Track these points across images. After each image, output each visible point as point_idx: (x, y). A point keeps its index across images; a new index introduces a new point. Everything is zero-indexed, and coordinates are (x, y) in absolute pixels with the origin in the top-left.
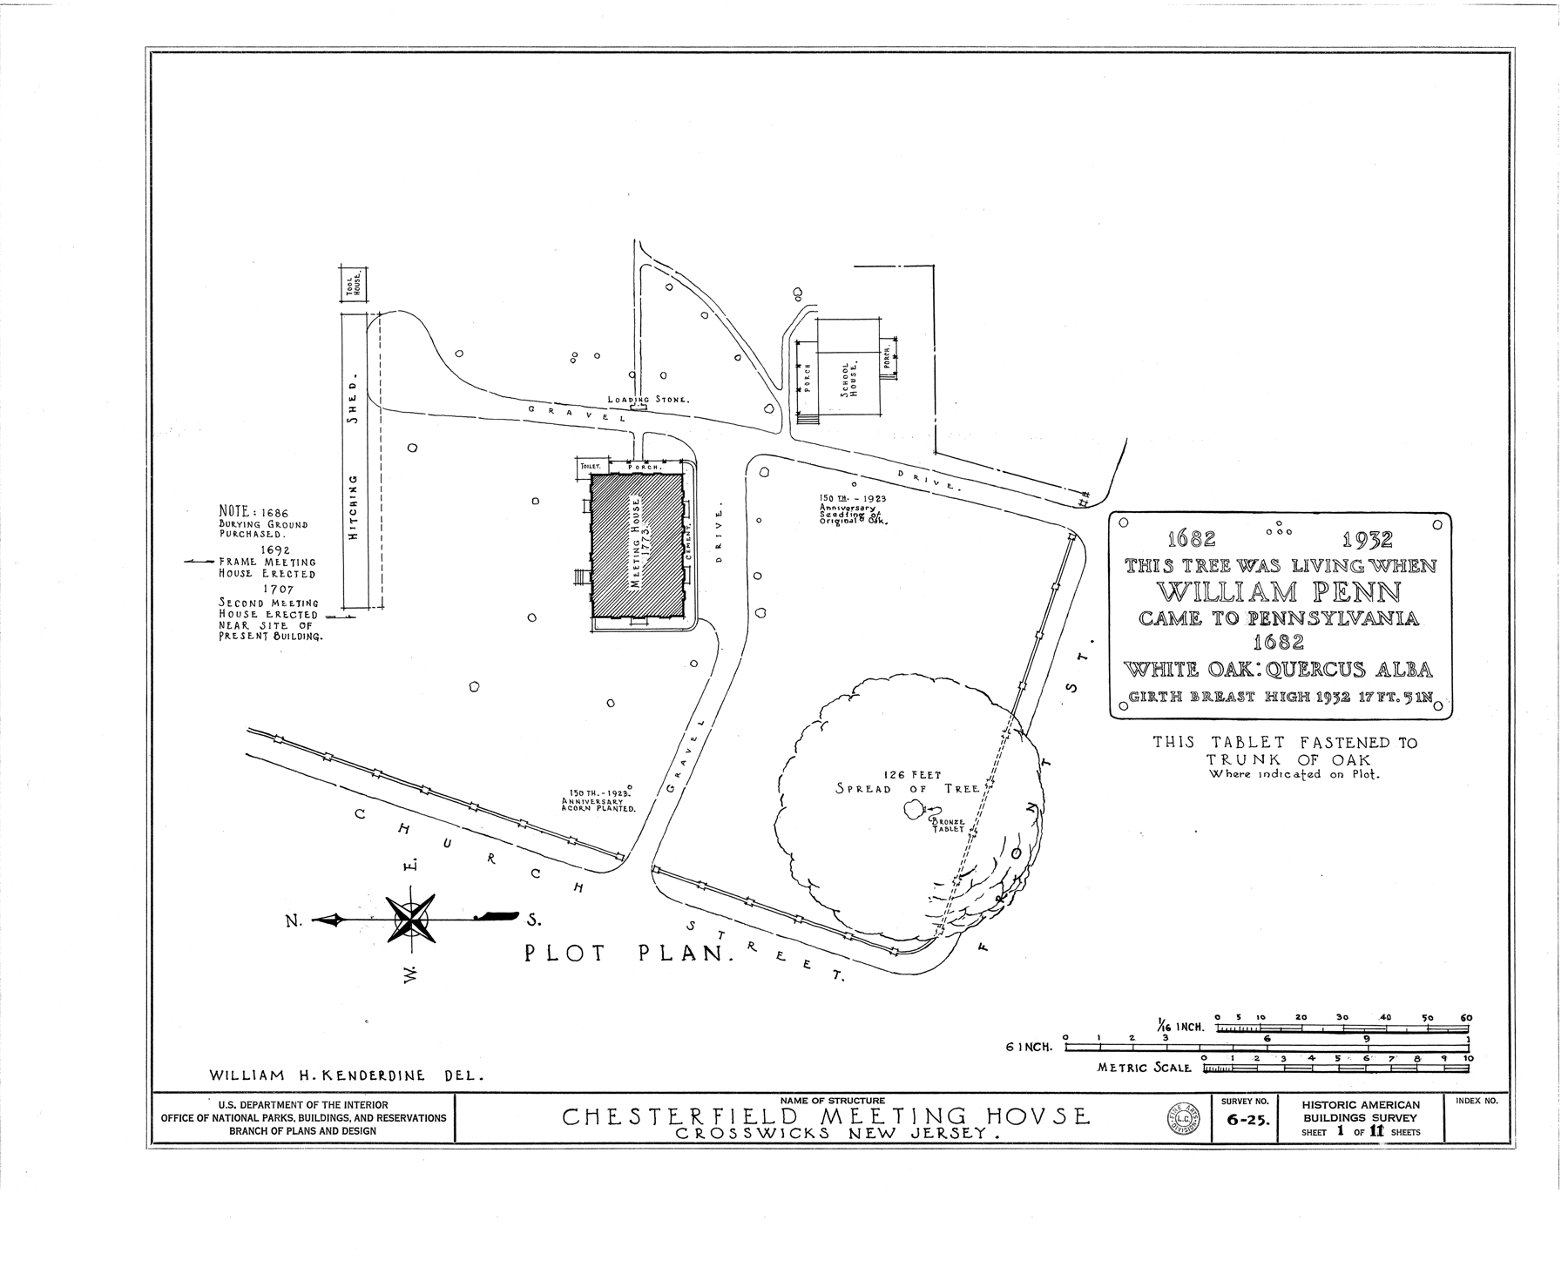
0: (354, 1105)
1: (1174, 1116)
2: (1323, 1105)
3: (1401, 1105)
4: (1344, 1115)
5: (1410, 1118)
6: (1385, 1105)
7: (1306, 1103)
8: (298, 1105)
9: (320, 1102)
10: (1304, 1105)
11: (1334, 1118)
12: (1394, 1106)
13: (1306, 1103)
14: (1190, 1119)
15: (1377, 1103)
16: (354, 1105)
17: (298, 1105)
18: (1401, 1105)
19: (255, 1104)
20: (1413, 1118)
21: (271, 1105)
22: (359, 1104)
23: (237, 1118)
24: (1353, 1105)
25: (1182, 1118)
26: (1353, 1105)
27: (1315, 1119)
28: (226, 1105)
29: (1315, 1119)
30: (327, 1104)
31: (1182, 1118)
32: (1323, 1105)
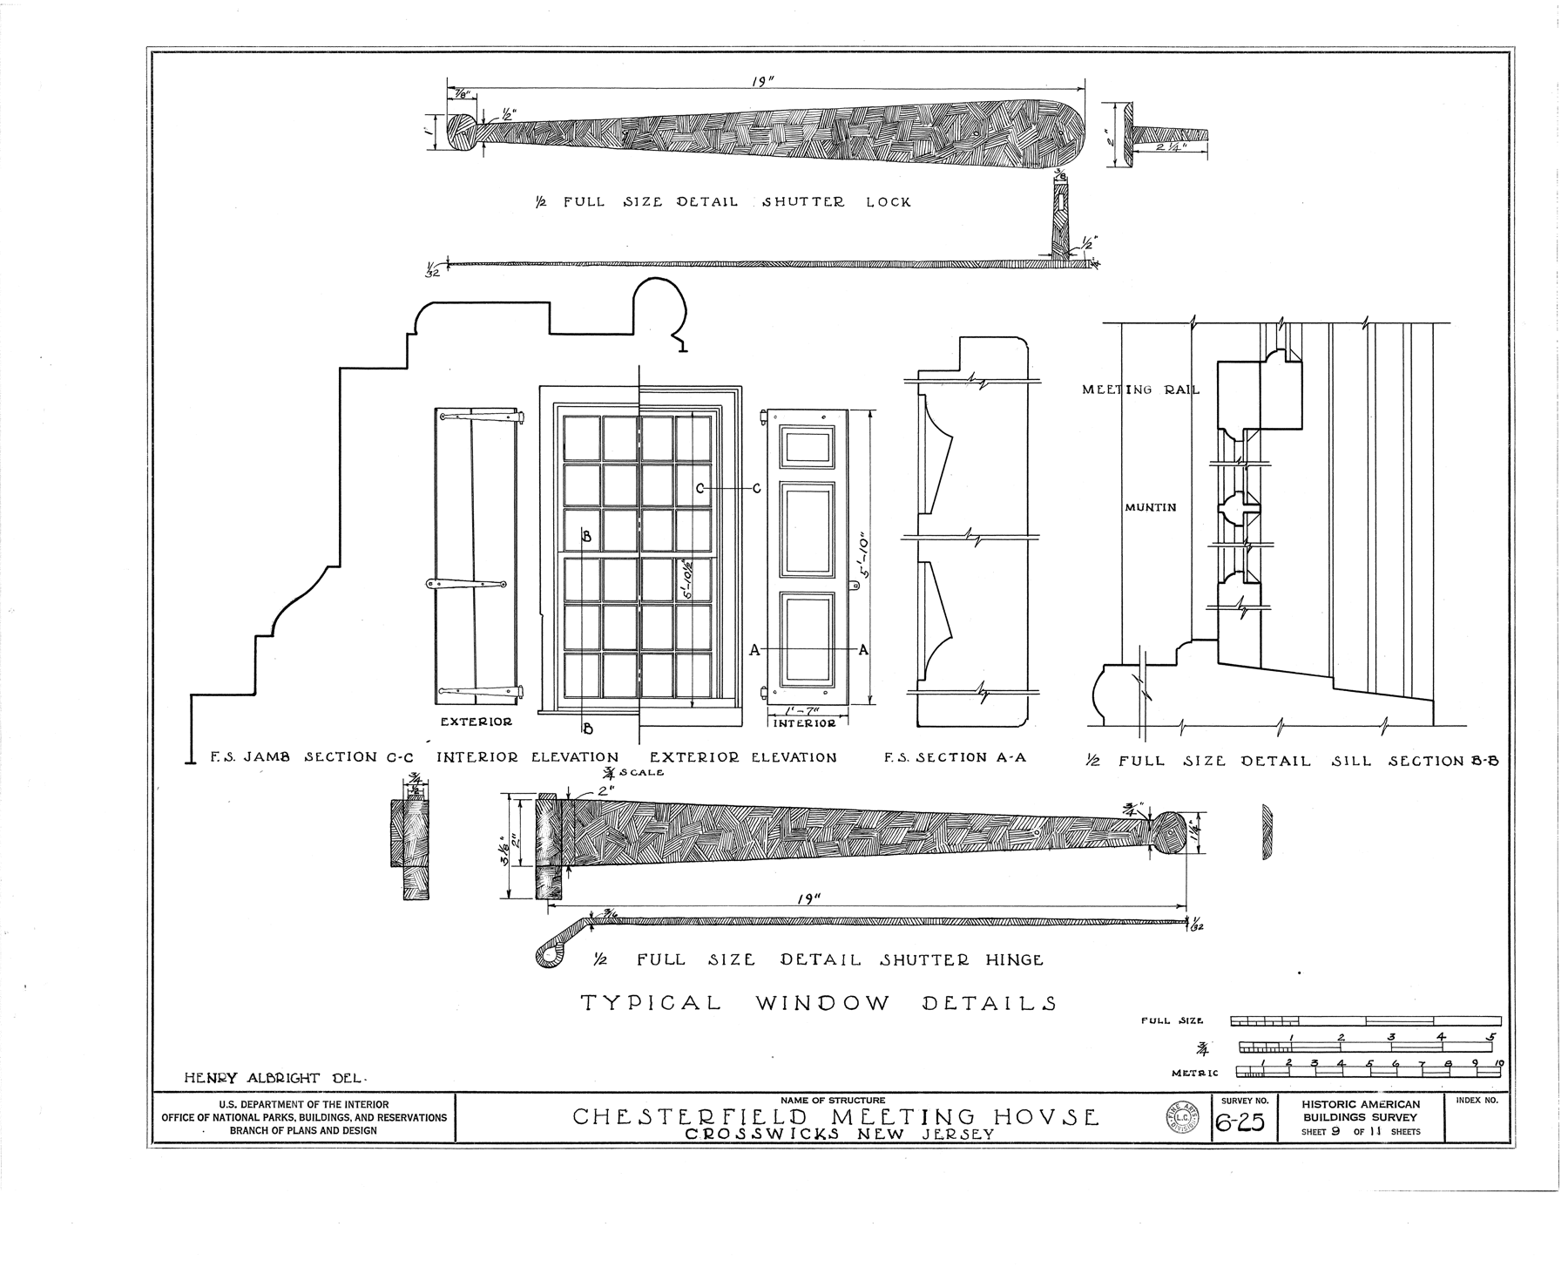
1: (1173, 1116)
2: (1322, 1104)
3: (1401, 1104)
4: (1344, 1115)
5: (1410, 1118)
6: (1385, 1105)
7: (1306, 1102)
8: (299, 1104)
9: (321, 1102)
11: (1334, 1117)
12: (1344, 1105)
14: (1189, 1117)
15: (1376, 1102)
18: (1401, 1104)
19: (256, 1103)
20: (1413, 1118)
21: (272, 1105)
22: (360, 1104)
23: (379, 1104)
24: (1352, 1104)
26: (1352, 1104)
27: (1315, 1118)
28: (227, 1104)
29: (1315, 1118)
30: (328, 1104)
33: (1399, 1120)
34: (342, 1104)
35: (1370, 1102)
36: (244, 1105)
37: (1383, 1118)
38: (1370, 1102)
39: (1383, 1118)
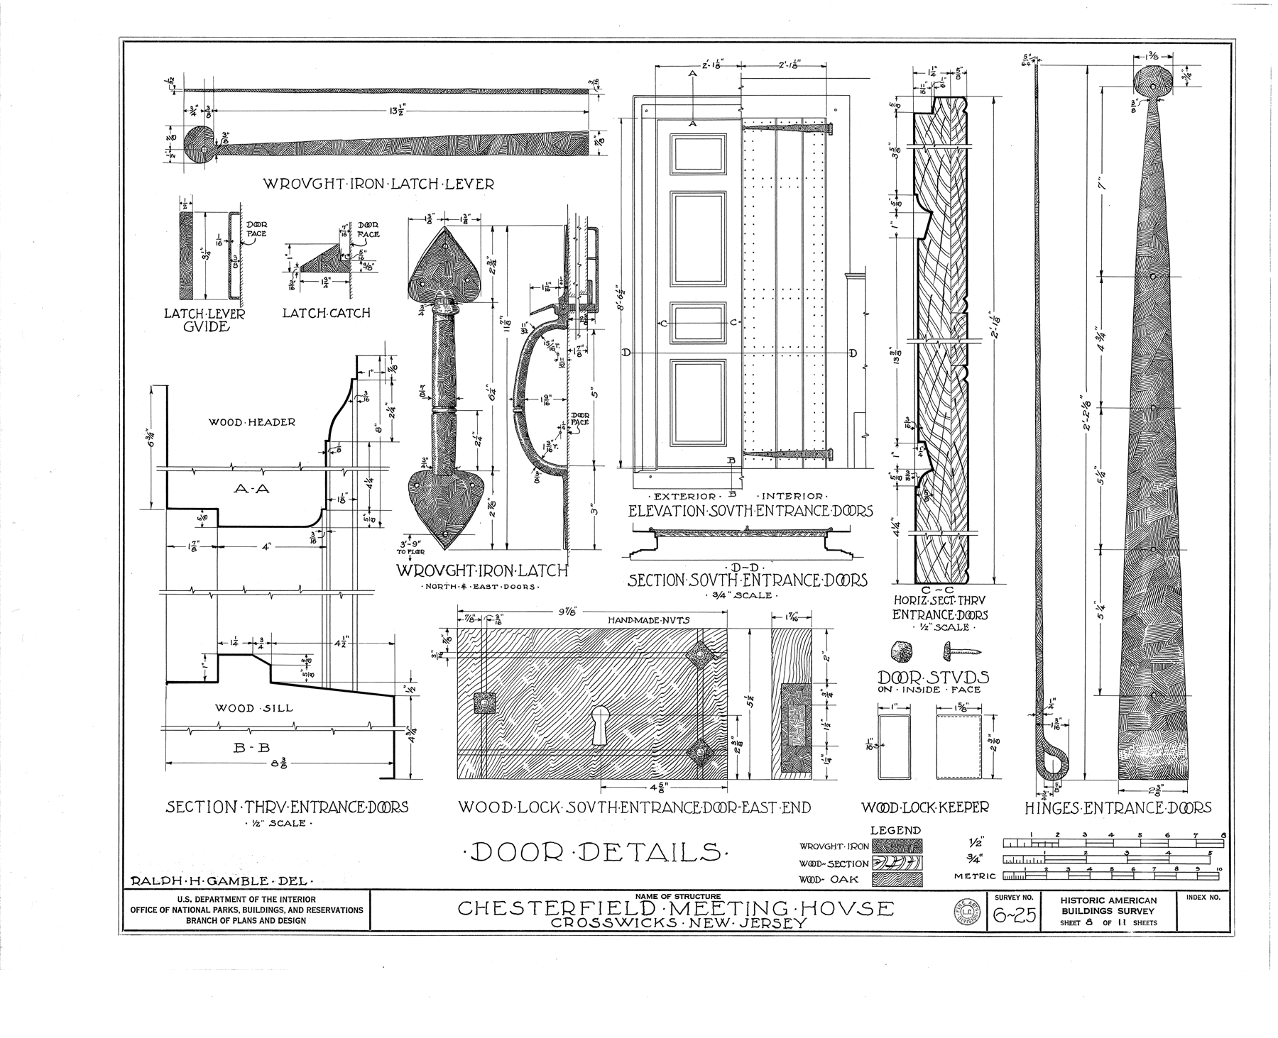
0: (288, 899)
2: (1077, 900)
6: (1128, 901)
7: (1064, 899)
8: (242, 899)
9: (260, 897)
11: (1087, 911)
13: (1064, 899)
14: (972, 912)
15: (1121, 899)
16: (288, 899)
17: (242, 899)
19: (207, 898)
21: (220, 900)
22: (292, 899)
23: (193, 910)
24: (1102, 900)
25: (966, 912)
26: (1102, 900)
27: (1071, 912)
28: (184, 899)
29: (1071, 912)
30: (266, 899)
31: (966, 912)
33: (1140, 913)
35: (1116, 899)
36: (198, 899)
37: (1127, 911)
38: (1116, 899)
39: (1127, 911)
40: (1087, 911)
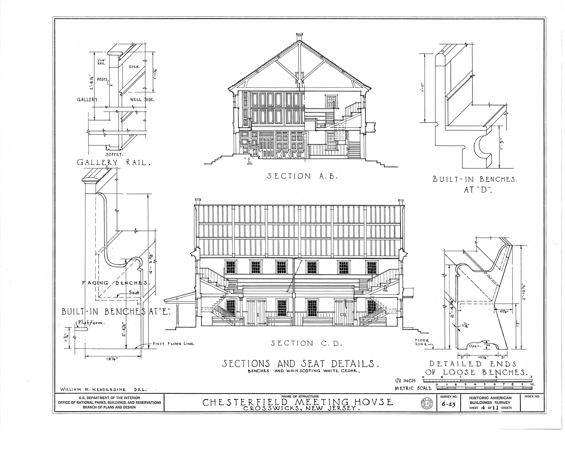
0: (128, 398)
2: (477, 398)
3: (505, 398)
5: (508, 403)
6: (499, 398)
7: (471, 397)
8: (108, 398)
9: (116, 397)
10: (470, 398)
11: (481, 403)
12: (502, 398)
13: (471, 397)
15: (496, 397)
16: (128, 398)
17: (108, 398)
18: (505, 398)
19: (92, 397)
21: (98, 398)
22: (129, 398)
24: (487, 398)
26: (487, 398)
27: (474, 403)
28: (82, 398)
29: (474, 403)
30: (118, 398)
32: (477, 398)
33: (504, 404)
34: (123, 398)
35: (494, 397)
36: (125, 407)
37: (498, 403)
38: (494, 397)
39: (498, 403)
40: (481, 403)
